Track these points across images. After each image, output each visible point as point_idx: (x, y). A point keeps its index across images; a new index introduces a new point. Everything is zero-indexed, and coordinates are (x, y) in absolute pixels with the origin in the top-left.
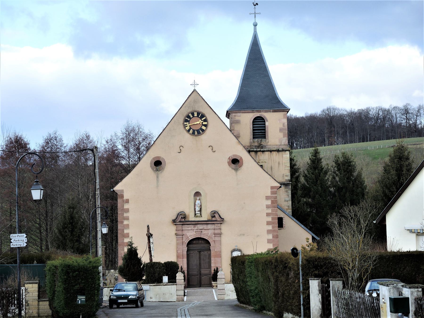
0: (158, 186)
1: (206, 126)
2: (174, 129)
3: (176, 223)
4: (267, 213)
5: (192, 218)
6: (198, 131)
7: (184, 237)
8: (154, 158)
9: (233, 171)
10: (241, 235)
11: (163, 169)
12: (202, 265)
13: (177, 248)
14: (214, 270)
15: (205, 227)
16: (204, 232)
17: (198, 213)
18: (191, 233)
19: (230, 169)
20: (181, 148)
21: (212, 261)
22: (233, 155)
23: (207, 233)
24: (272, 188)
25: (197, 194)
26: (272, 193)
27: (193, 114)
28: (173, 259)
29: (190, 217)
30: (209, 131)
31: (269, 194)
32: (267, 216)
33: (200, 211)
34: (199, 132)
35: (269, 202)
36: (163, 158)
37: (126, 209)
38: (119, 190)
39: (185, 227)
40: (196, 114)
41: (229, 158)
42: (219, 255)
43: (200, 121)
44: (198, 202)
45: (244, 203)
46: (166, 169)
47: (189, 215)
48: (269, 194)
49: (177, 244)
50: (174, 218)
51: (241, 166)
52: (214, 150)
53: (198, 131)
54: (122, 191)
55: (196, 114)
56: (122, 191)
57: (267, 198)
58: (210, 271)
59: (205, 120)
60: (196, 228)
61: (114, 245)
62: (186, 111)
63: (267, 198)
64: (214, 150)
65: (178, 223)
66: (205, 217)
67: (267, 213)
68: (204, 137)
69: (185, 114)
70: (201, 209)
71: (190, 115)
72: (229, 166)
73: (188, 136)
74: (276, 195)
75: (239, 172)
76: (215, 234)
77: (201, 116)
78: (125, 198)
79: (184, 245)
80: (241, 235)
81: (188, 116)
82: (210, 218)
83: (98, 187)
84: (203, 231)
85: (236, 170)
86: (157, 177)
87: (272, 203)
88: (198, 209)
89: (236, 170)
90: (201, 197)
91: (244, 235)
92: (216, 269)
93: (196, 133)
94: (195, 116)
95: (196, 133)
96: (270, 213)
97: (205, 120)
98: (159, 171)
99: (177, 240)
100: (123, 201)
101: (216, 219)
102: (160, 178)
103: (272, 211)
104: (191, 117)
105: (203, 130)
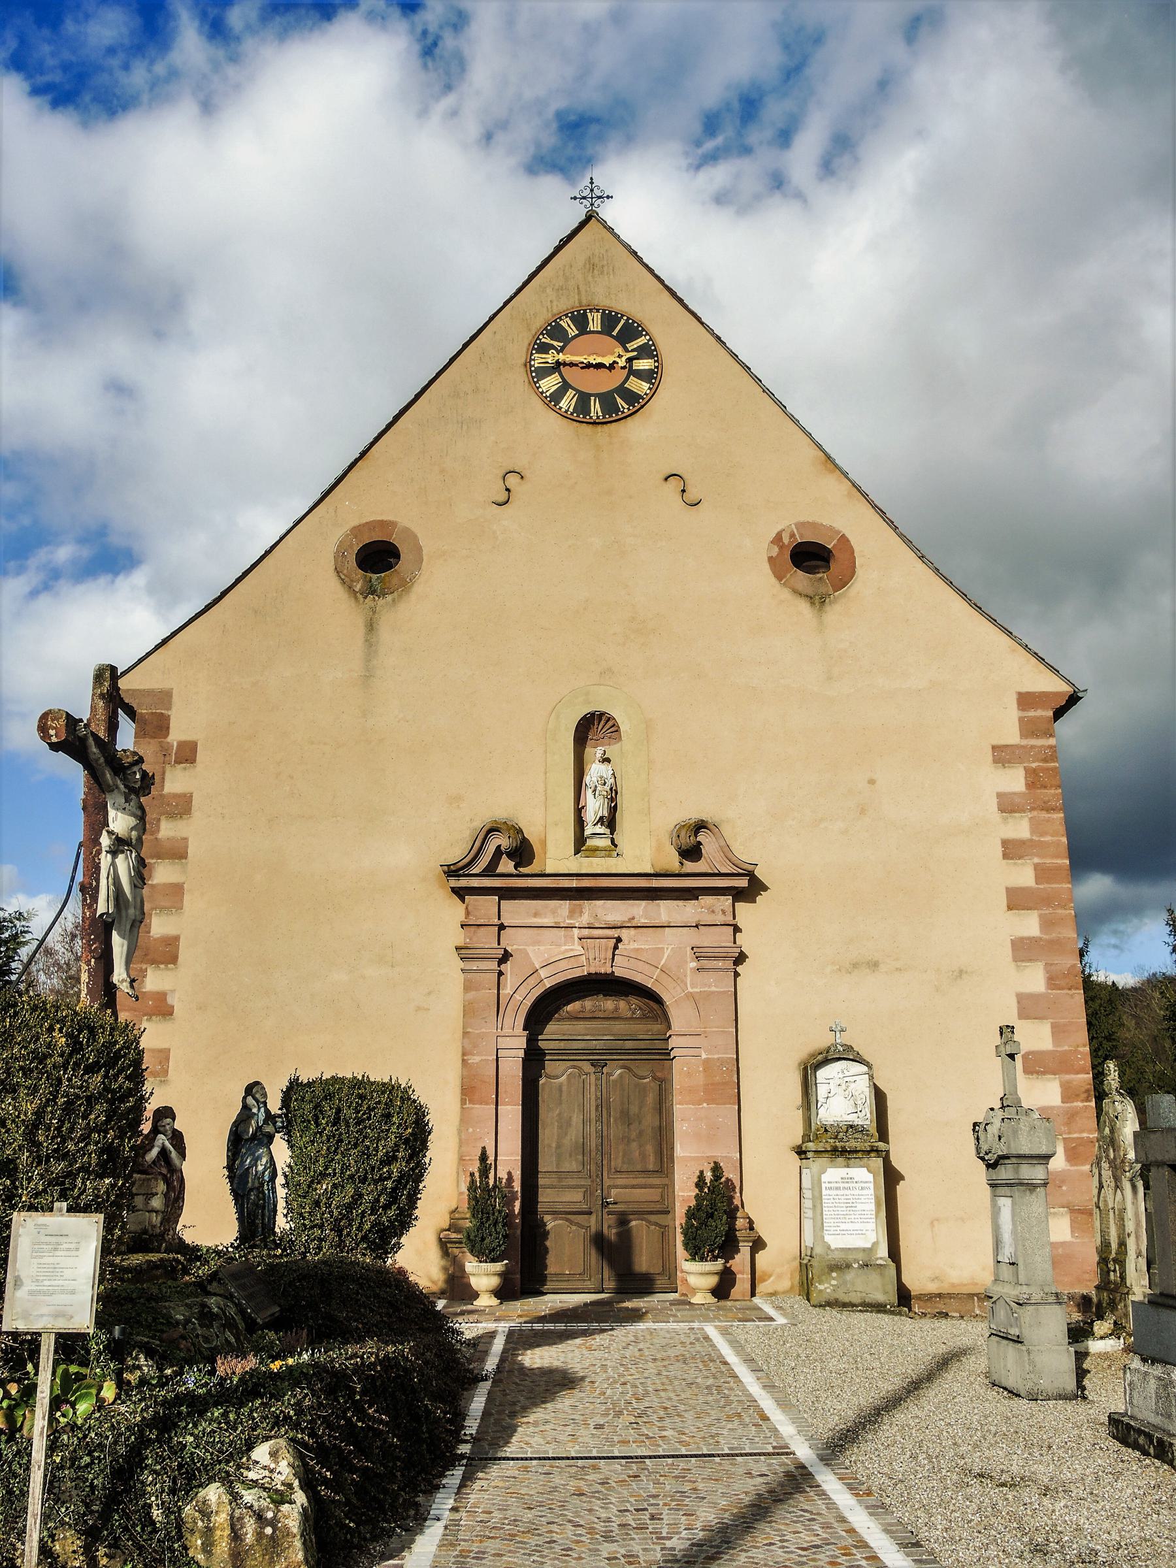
0: (368, 676)
1: (650, 376)
2: (476, 391)
3: (463, 882)
4: (1005, 843)
5: (557, 857)
6: (607, 401)
7: (507, 967)
8: (356, 531)
9: (803, 606)
10: (855, 965)
11: (406, 585)
12: (639, 1168)
13: (465, 1034)
14: (700, 1183)
15: (638, 910)
16: (631, 942)
17: (599, 829)
18: (552, 945)
19: (786, 594)
20: (512, 480)
21: (681, 1128)
22: (800, 525)
23: (658, 946)
24: (1026, 700)
25: (591, 728)
26: (1028, 728)
27: (580, 320)
28: (1049, 1026)
29: (551, 851)
30: (666, 402)
31: (1011, 735)
32: (1006, 856)
33: (610, 821)
34: (619, 405)
35: (1014, 781)
36: (407, 531)
37: (176, 796)
38: (150, 693)
39: (516, 911)
40: (595, 322)
41: (778, 539)
42: (728, 1087)
43: (620, 350)
44: (595, 771)
45: (872, 782)
46: (418, 589)
47: (544, 843)
48: (1011, 735)
49: (469, 1011)
50: (456, 854)
51: (842, 583)
52: (692, 495)
53: (607, 401)
54: (165, 697)
55: (595, 322)
56: (165, 697)
57: (1002, 755)
58: (668, 1189)
59: (647, 351)
60: (585, 919)
61: (1020, 1247)
62: (541, 307)
63: (1002, 755)
64: (692, 495)
65: (475, 883)
66: (642, 849)
67: (1005, 843)
68: (636, 431)
69: (539, 323)
70: (613, 810)
71: (566, 323)
72: (779, 578)
73: (548, 423)
74: (1052, 741)
75: (834, 613)
76: (699, 954)
77: (622, 328)
78: (176, 735)
79: (508, 1021)
80: (855, 965)
81: (555, 330)
82: (672, 861)
83: (742, 1370)
84: (624, 934)
85: (819, 601)
86: (371, 627)
87: (1030, 785)
88: (594, 807)
89: (819, 601)
90: (612, 751)
91: (874, 965)
92: (708, 1175)
93: (596, 408)
94: (591, 327)
95: (596, 408)
96: (1022, 843)
97: (647, 351)
98: (383, 594)
99: (467, 987)
100: (165, 751)
101: (707, 876)
102: (385, 633)
103: (1035, 826)
104: (572, 331)
105: (632, 398)
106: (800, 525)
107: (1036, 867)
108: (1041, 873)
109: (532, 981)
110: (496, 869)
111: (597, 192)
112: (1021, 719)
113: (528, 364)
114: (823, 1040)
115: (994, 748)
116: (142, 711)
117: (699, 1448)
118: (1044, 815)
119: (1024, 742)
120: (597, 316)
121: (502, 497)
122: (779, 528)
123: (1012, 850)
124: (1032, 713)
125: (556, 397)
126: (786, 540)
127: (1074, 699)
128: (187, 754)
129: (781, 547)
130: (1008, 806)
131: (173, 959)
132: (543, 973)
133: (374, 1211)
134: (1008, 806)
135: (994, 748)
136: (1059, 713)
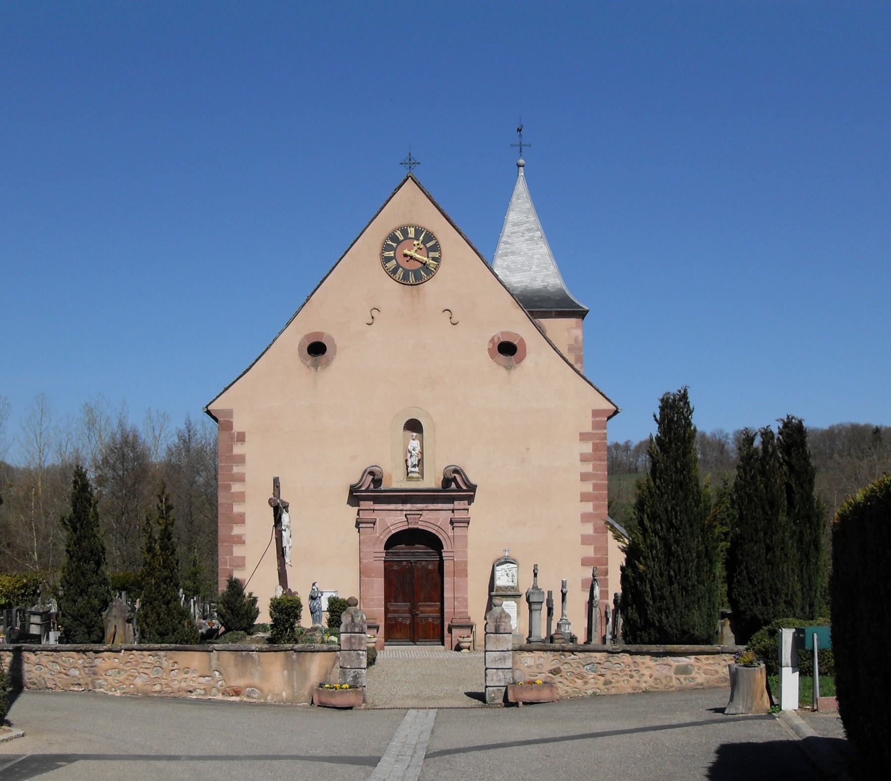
6: (416, 273)
11: (328, 363)
18: (394, 519)
20: (375, 313)
22: (503, 333)
23: (435, 519)
24: (596, 413)
26: (596, 425)
31: (588, 428)
32: (581, 480)
35: (588, 448)
53: (416, 273)
54: (230, 413)
56: (230, 413)
57: (584, 437)
63: (584, 437)
64: (454, 320)
66: (432, 480)
68: (429, 287)
71: (398, 234)
87: (594, 450)
106: (503, 333)
107: (594, 484)
108: (596, 487)
109: (387, 531)
110: (368, 492)
111: (413, 161)
112: (593, 422)
113: (381, 254)
114: (500, 554)
115: (581, 434)
116: (220, 419)
117: (349, 654)
118: (599, 462)
119: (596, 432)
120: (413, 229)
121: (370, 321)
122: (494, 334)
123: (584, 477)
124: (597, 419)
125: (395, 271)
126: (496, 340)
127: (616, 412)
128: (241, 438)
129: (494, 344)
130: (584, 459)
131: (243, 522)
132: (391, 528)
133: (75, 618)
134: (584, 459)
135: (581, 434)
136: (609, 418)
